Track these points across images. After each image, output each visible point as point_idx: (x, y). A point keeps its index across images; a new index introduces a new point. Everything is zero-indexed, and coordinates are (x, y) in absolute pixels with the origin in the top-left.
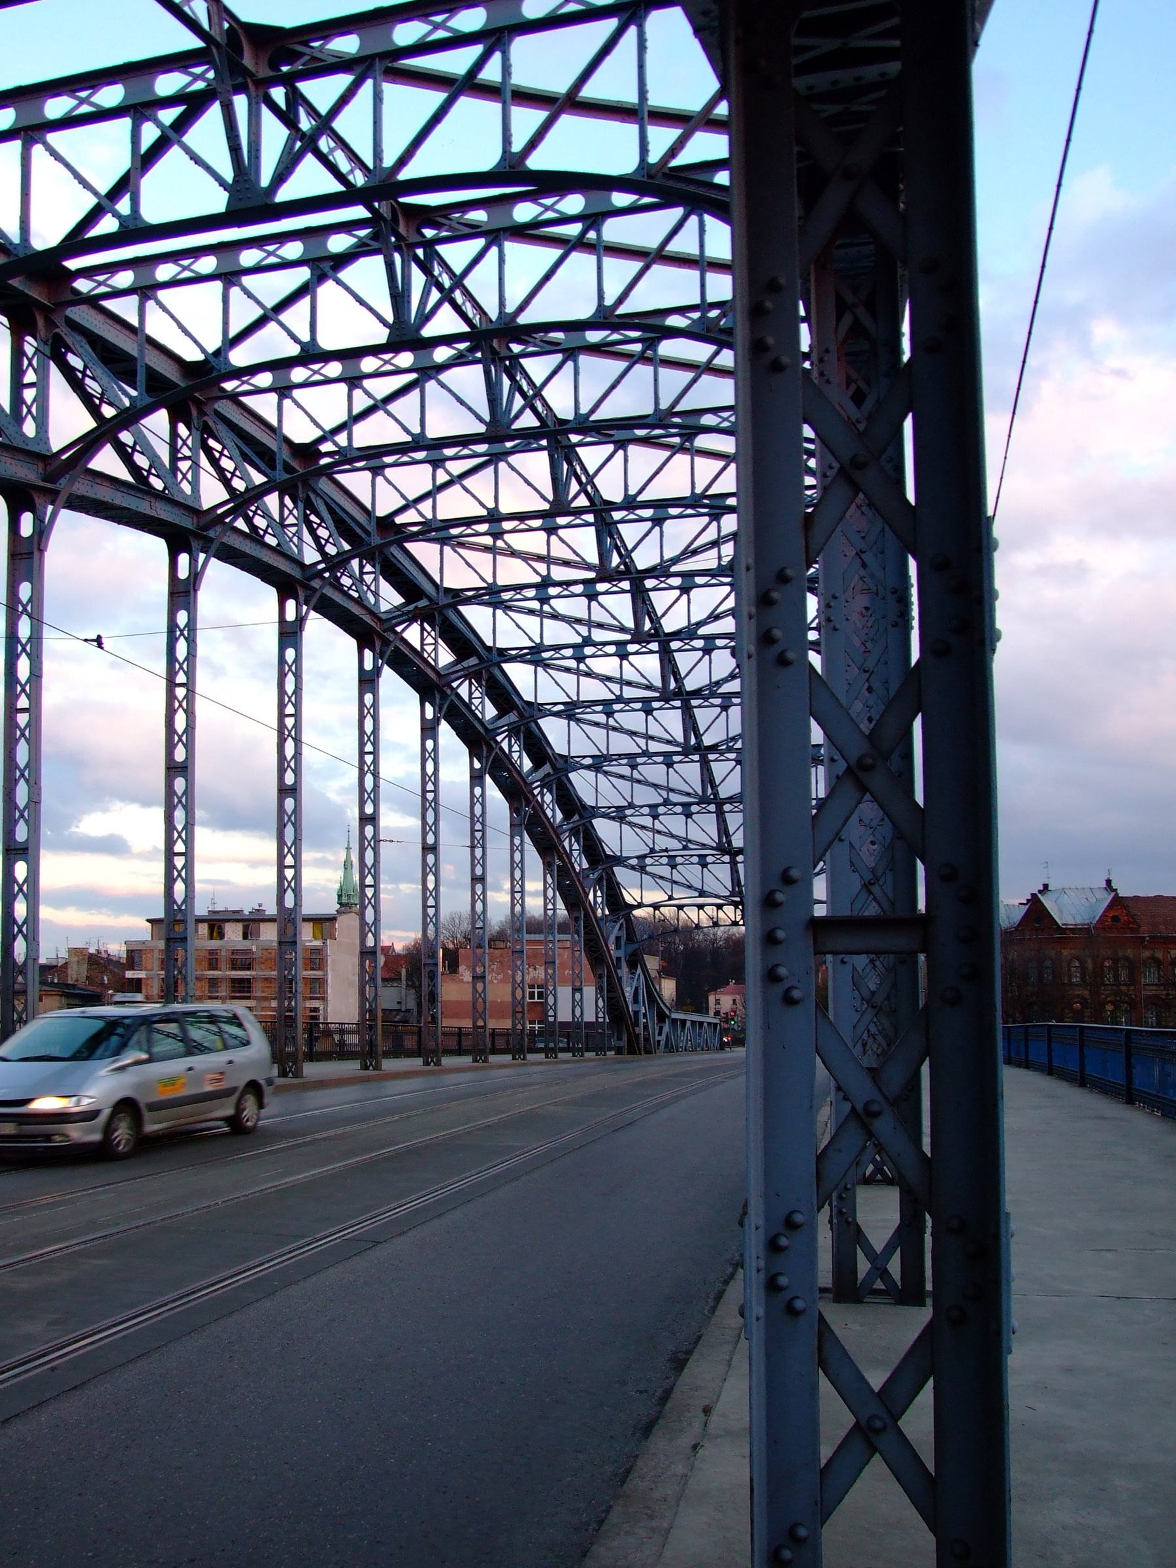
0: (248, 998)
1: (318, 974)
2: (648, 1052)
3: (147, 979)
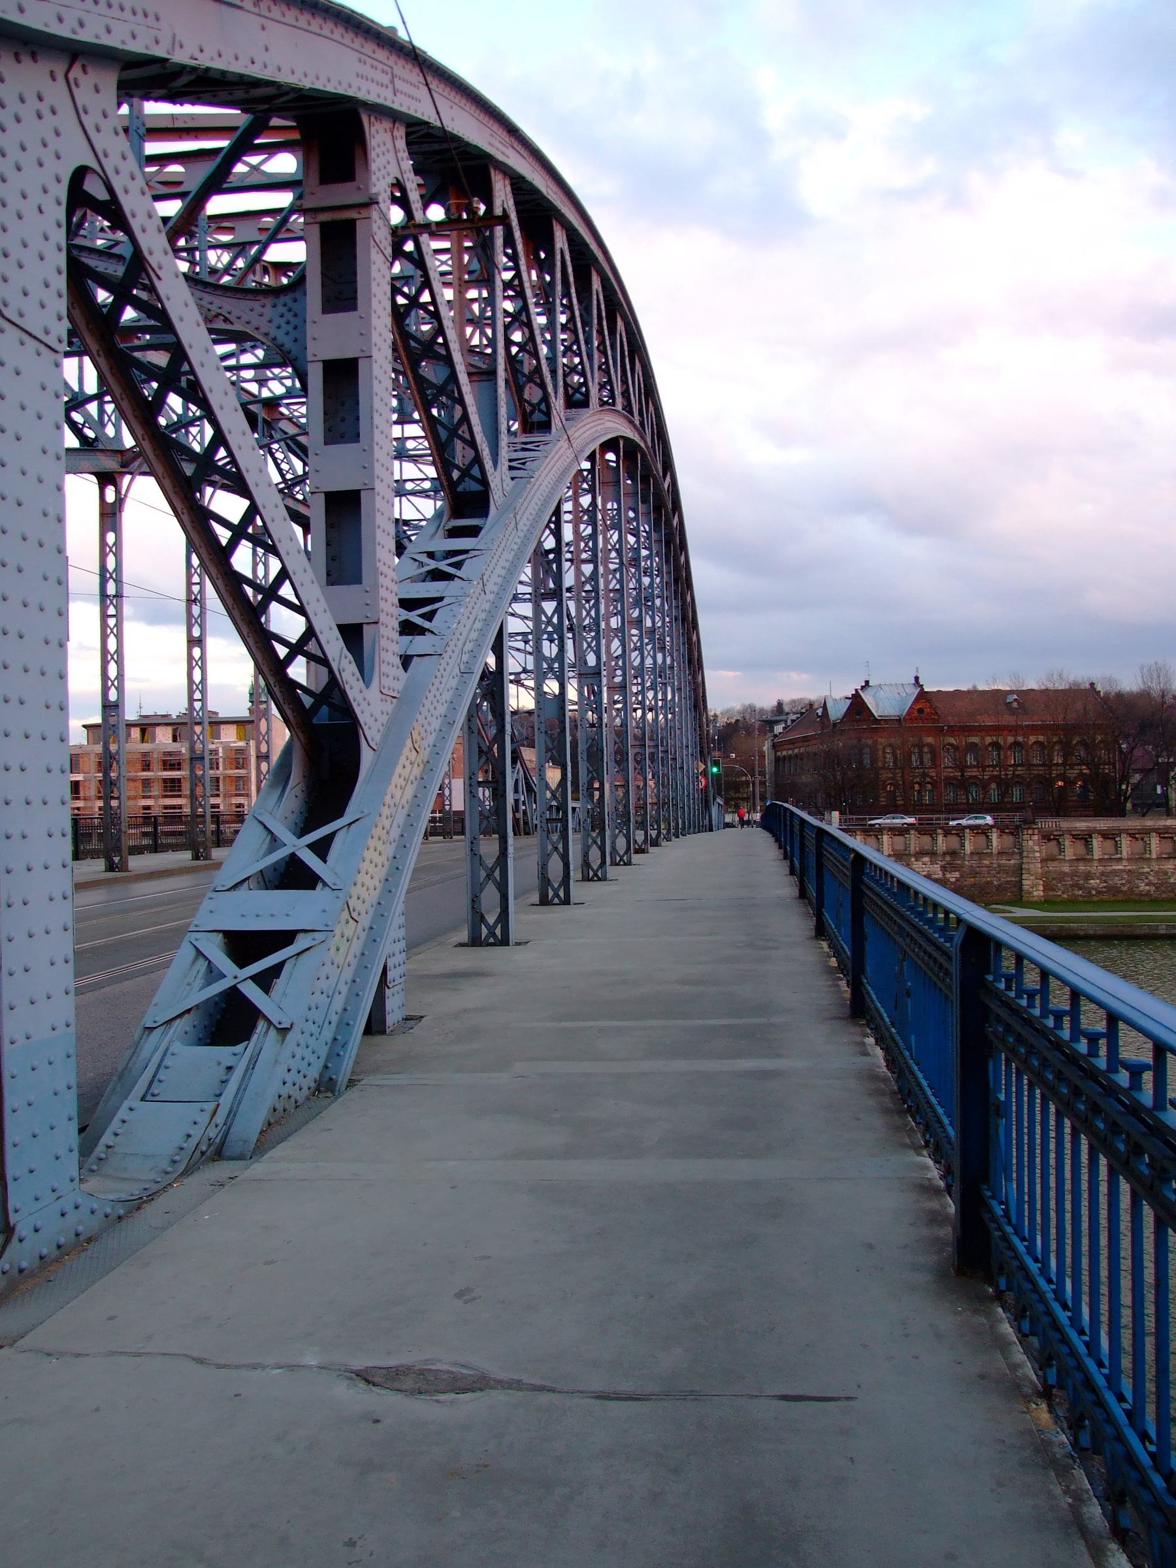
0: (180, 796)
1: (242, 772)
2: (527, 833)
3: (85, 781)
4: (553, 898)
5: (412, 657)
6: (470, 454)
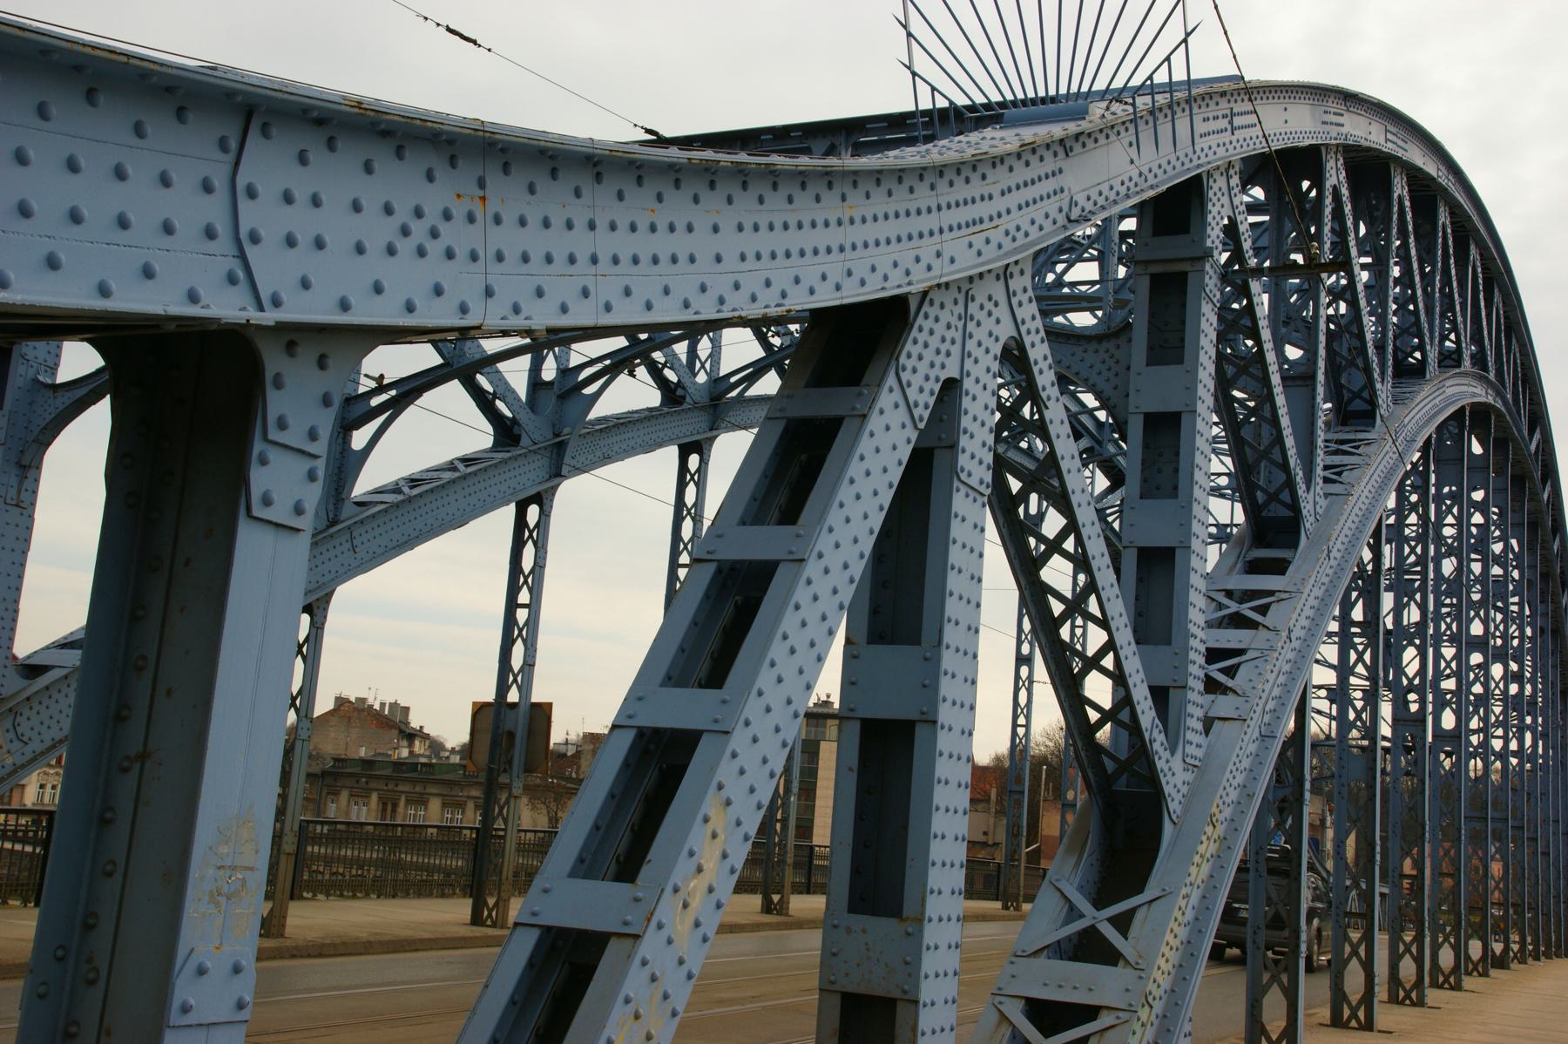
4: (1349, 1019)
5: (1214, 719)
6: (1281, 477)
